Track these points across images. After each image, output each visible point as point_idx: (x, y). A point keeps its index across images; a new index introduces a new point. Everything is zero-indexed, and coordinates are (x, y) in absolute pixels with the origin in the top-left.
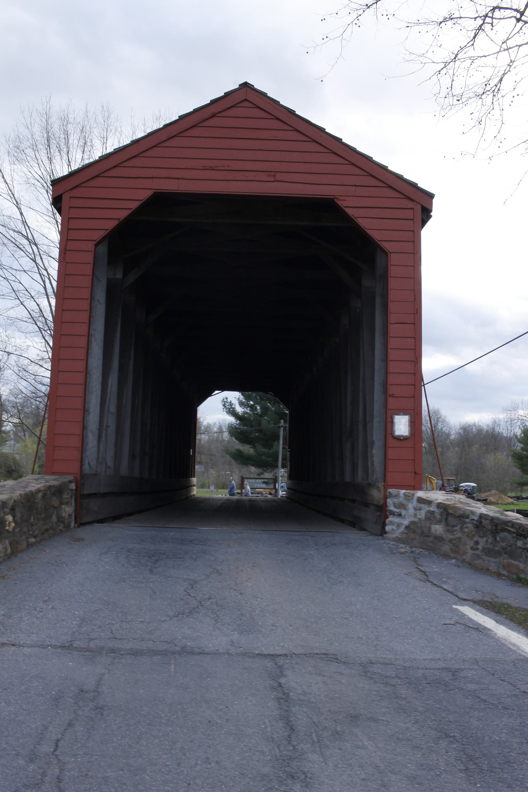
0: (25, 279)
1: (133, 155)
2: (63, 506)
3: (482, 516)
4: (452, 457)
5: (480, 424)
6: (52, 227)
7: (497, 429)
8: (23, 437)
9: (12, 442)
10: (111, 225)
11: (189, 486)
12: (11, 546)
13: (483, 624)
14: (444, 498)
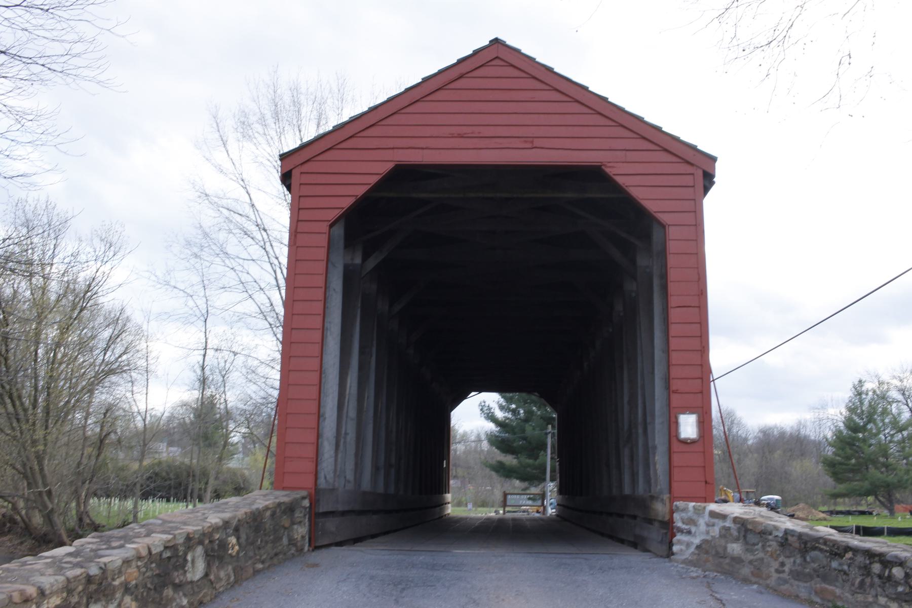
0: (254, 269)
2: (295, 527)
4: (750, 466)
5: (783, 425)
7: (803, 432)
9: (241, 456)
10: (347, 203)
11: (442, 504)
12: (234, 572)
14: (742, 511)
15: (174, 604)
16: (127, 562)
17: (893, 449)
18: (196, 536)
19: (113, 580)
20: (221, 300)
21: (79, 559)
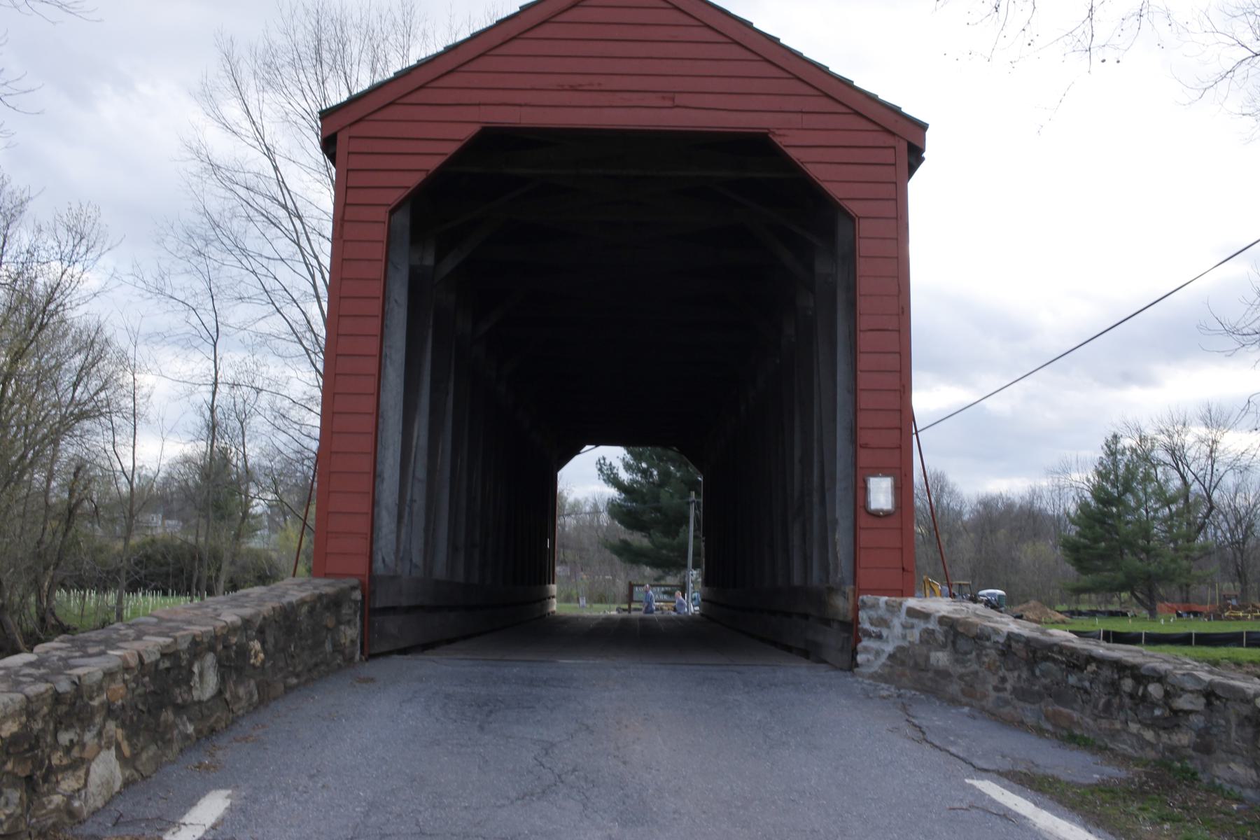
0: (282, 271)
1: (450, 68)
2: (342, 627)
4: (965, 547)
6: (325, 190)
7: (1037, 504)
8: (283, 524)
10: (414, 180)
11: (545, 598)
13: (1014, 808)
14: (950, 608)
15: (176, 732)
16: (109, 675)
17: (1157, 529)
18: (205, 640)
19: (91, 698)
20: (236, 314)
21: (42, 671)
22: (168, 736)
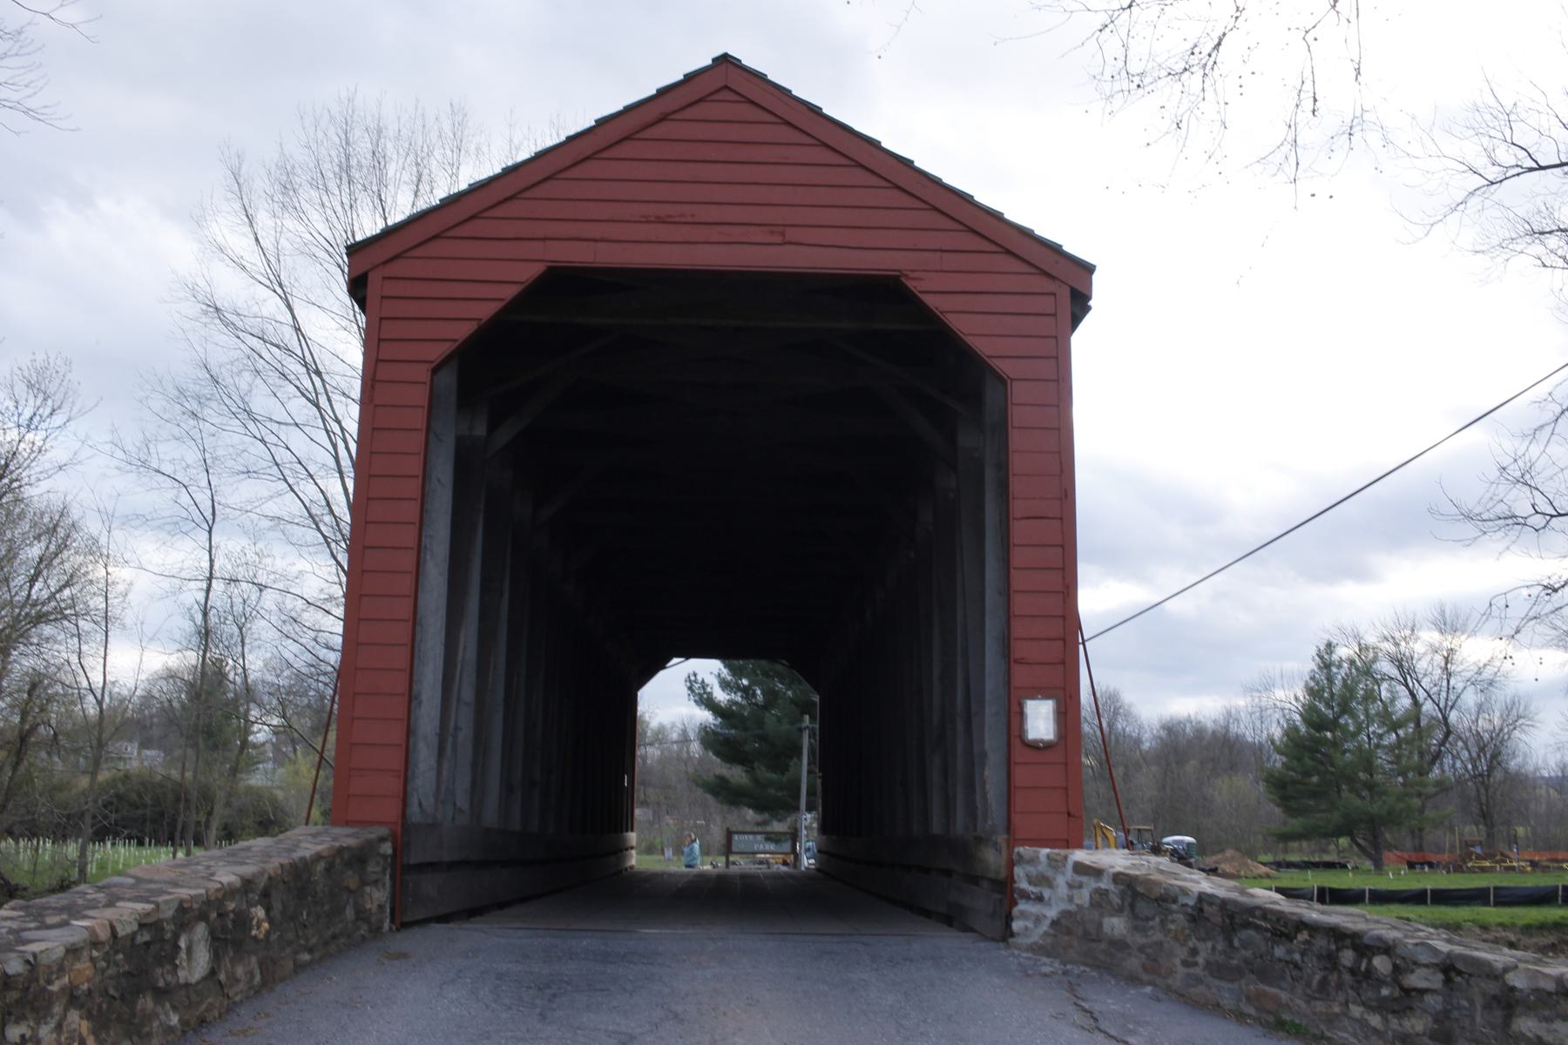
0: (296, 440)
2: (368, 889)
3: (1203, 898)
4: (1145, 784)
7: (1234, 729)
9: (270, 765)
10: (463, 331)
11: (621, 849)
14: (1128, 863)
15: (156, 1024)
16: (73, 951)
18: (195, 906)
19: (50, 982)
22: (146, 1029)
